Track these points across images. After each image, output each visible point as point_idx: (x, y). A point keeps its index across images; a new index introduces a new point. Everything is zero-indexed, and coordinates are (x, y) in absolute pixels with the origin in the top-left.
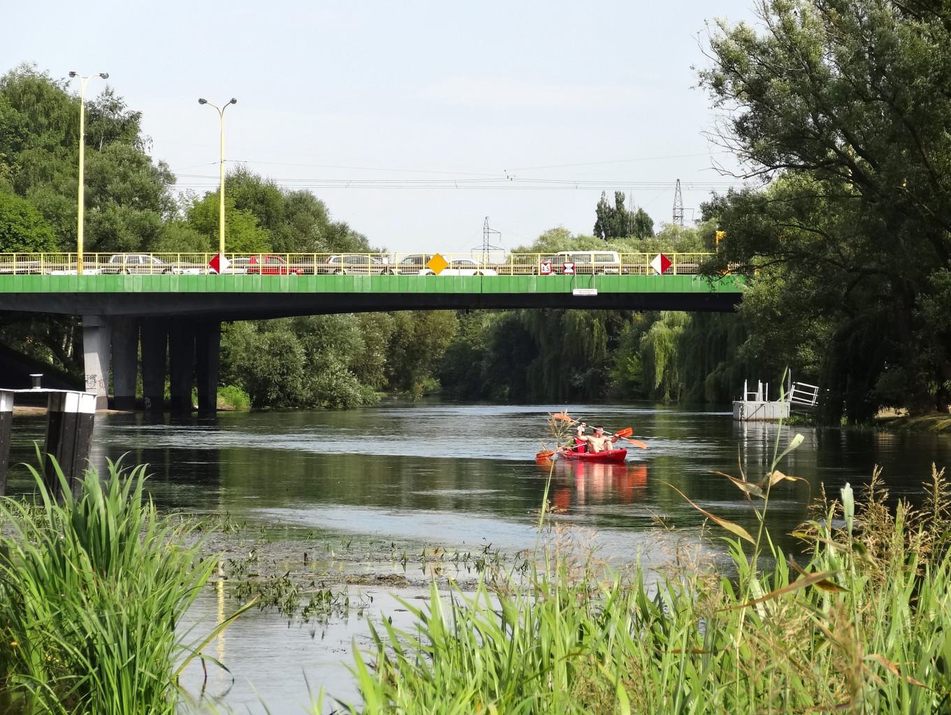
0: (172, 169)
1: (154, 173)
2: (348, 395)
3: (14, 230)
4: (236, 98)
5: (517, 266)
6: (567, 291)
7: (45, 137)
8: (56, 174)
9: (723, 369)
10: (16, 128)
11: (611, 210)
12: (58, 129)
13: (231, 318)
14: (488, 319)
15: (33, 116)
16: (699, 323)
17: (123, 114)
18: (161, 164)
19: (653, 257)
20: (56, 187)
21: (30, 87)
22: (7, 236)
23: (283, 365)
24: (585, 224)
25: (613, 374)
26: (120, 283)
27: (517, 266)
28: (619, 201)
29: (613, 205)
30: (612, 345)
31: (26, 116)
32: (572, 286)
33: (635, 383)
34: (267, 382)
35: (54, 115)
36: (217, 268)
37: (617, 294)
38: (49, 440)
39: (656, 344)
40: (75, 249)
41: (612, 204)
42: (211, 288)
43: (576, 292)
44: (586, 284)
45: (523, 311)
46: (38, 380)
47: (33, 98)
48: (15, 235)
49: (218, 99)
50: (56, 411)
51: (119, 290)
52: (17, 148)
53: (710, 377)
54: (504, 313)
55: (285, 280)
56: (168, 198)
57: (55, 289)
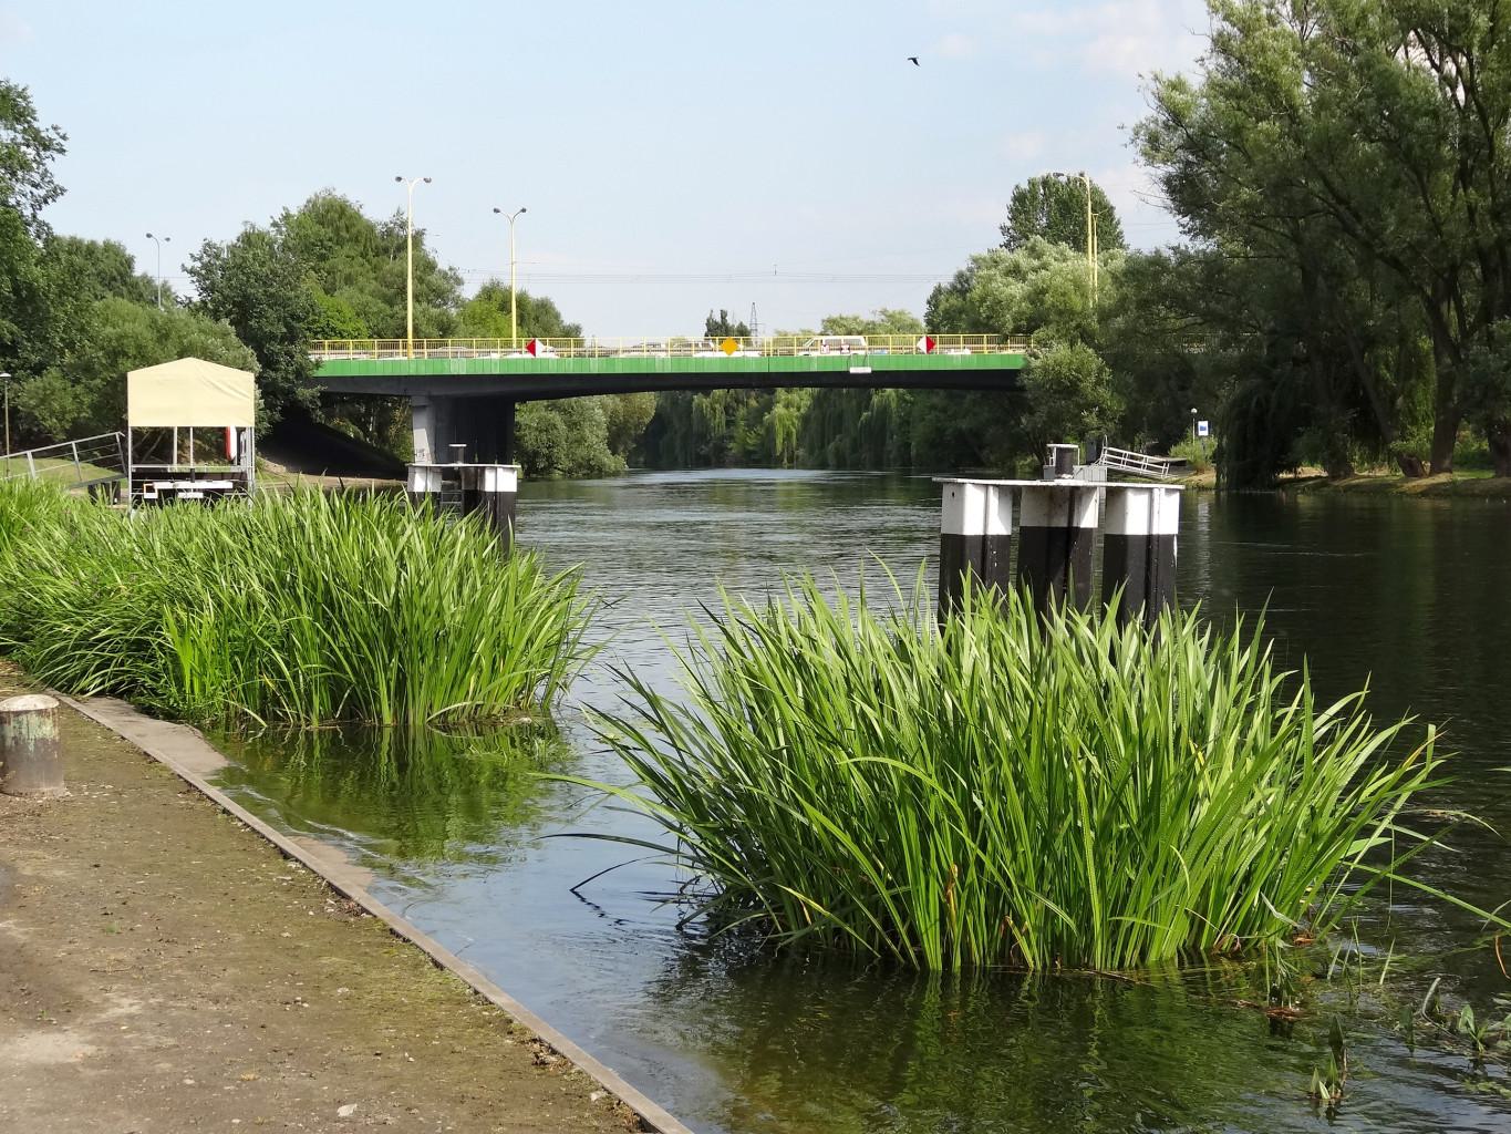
0: (460, 274)
1: (445, 276)
2: (605, 465)
3: (332, 325)
6: (844, 369)
7: (346, 248)
8: (360, 279)
10: (321, 241)
11: (716, 323)
12: (357, 241)
13: (525, 397)
14: (648, 401)
15: (337, 231)
16: (818, 402)
18: (451, 269)
19: (919, 339)
20: (361, 291)
21: (332, 206)
22: (327, 330)
23: (549, 440)
24: (697, 333)
25: (731, 445)
26: (447, 367)
28: (724, 315)
29: (718, 319)
30: (729, 423)
31: (330, 232)
32: (848, 365)
33: (754, 452)
34: (536, 454)
35: (354, 230)
36: (533, 352)
37: (887, 372)
39: (777, 421)
40: (404, 335)
41: (718, 319)
42: (528, 371)
43: (853, 370)
46: (461, 453)
47: (336, 216)
48: (333, 329)
50: (1063, 523)
51: (446, 373)
52: (323, 258)
53: (831, 447)
57: (388, 372)
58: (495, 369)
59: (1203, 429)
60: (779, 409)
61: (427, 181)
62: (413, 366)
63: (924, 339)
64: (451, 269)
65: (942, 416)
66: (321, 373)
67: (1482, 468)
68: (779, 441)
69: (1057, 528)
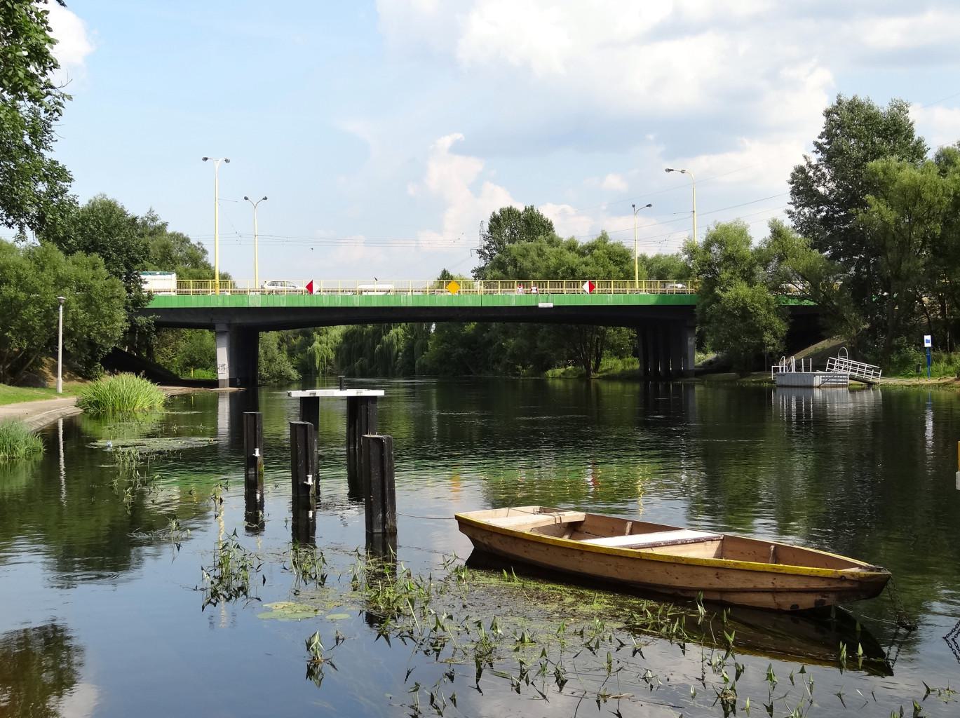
4: (267, 197)
5: (465, 290)
6: (534, 304)
9: (362, 361)
17: (158, 223)
19: (584, 283)
26: (246, 301)
27: (465, 290)
38: (303, 411)
43: (540, 305)
44: (545, 300)
45: (370, 326)
49: (255, 198)
51: (246, 305)
54: (351, 326)
55: (357, 298)
56: (206, 262)
58: (283, 303)
59: (928, 341)
60: (316, 344)
61: (227, 161)
62: (220, 300)
63: (588, 283)
64: (199, 243)
65: (449, 346)
66: (152, 305)
67: (431, 378)
68: (318, 362)
69: (218, 402)
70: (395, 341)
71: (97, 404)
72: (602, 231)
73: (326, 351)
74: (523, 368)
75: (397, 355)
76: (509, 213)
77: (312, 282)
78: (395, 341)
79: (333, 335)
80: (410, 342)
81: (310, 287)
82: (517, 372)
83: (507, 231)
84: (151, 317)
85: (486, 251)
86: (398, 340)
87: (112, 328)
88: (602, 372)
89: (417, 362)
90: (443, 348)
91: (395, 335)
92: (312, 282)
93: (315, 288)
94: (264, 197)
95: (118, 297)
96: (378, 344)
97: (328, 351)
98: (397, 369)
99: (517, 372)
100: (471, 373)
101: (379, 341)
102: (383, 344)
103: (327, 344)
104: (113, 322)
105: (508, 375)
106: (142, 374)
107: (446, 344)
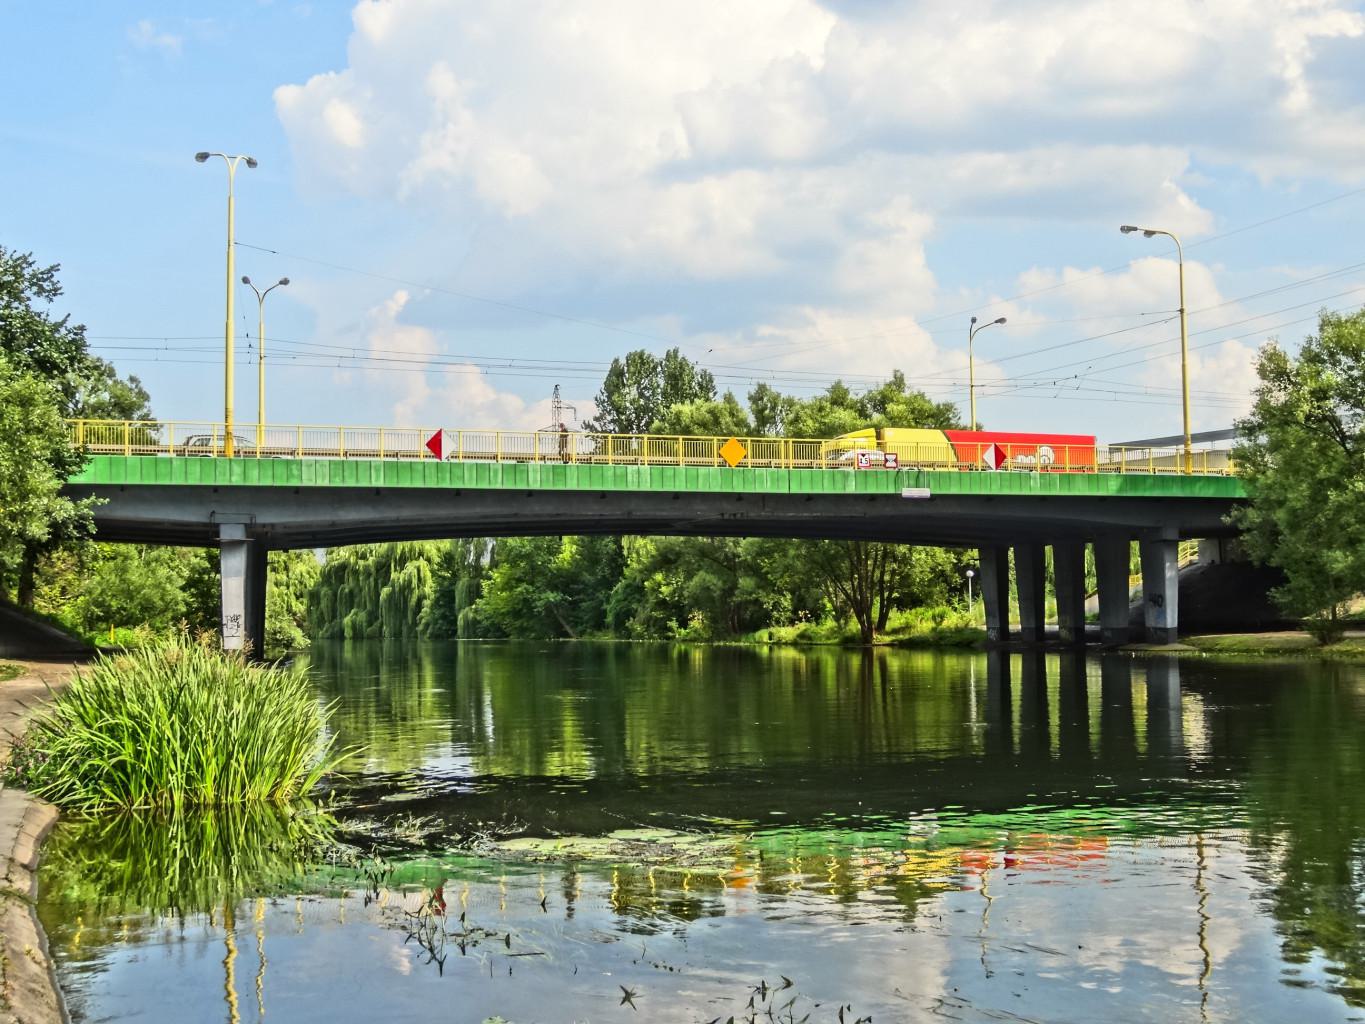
4: (290, 278)
19: (985, 448)
61: (251, 163)
64: (132, 379)
70: (415, 581)
71: (121, 777)
72: (896, 371)
73: (286, 598)
74: (680, 626)
75: (419, 606)
76: (640, 363)
77: (439, 434)
78: (415, 581)
79: (298, 572)
80: (446, 583)
81: (435, 445)
82: (670, 634)
83: (634, 392)
84: (86, 501)
85: (597, 425)
86: (419, 579)
87: (22, 512)
88: (895, 631)
89: (460, 616)
90: (521, 593)
91: (416, 571)
92: (439, 434)
93: (447, 448)
94: (281, 278)
95: (39, 431)
96: (385, 584)
97: (289, 598)
98: (420, 628)
99: (670, 634)
100: (567, 635)
101: (386, 580)
102: (393, 586)
103: (288, 588)
104: (24, 497)
105: (654, 639)
106: (1211, 708)
107: (525, 585)
